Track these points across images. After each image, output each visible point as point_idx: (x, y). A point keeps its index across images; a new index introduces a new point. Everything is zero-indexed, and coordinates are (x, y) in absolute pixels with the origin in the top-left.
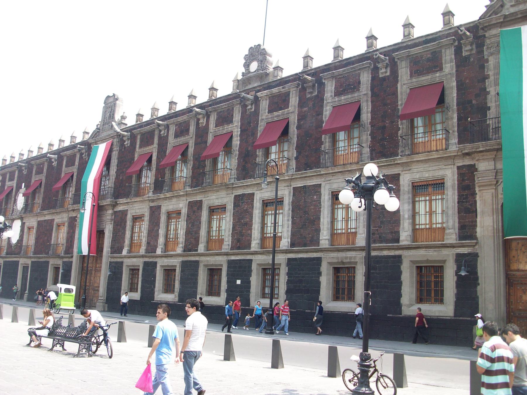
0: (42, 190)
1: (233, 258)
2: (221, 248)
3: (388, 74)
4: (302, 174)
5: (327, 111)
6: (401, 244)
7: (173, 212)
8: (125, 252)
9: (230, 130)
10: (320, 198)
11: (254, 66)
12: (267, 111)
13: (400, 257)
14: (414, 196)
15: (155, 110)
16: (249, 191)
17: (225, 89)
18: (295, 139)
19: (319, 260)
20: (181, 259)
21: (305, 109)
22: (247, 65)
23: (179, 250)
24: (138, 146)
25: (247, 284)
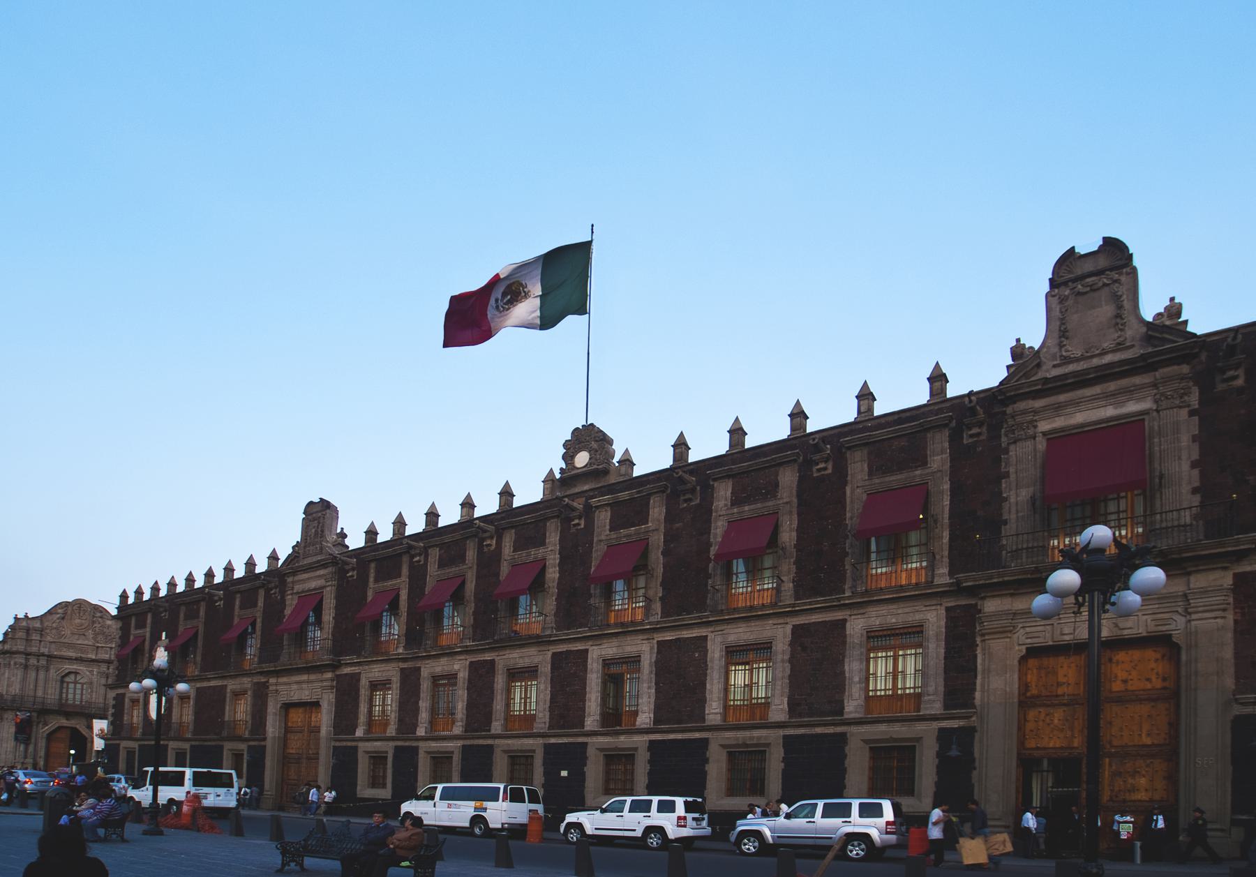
0: (200, 643)
1: (553, 741)
2: (385, 732)
3: (829, 471)
5: (719, 528)
6: (846, 716)
7: (443, 677)
8: (359, 733)
9: (540, 556)
10: (706, 655)
11: (582, 459)
13: (844, 735)
14: (728, 664)
16: (579, 646)
18: (660, 570)
19: (705, 742)
20: (460, 743)
22: (568, 457)
23: (458, 730)
24: (371, 579)
25: (578, 777)
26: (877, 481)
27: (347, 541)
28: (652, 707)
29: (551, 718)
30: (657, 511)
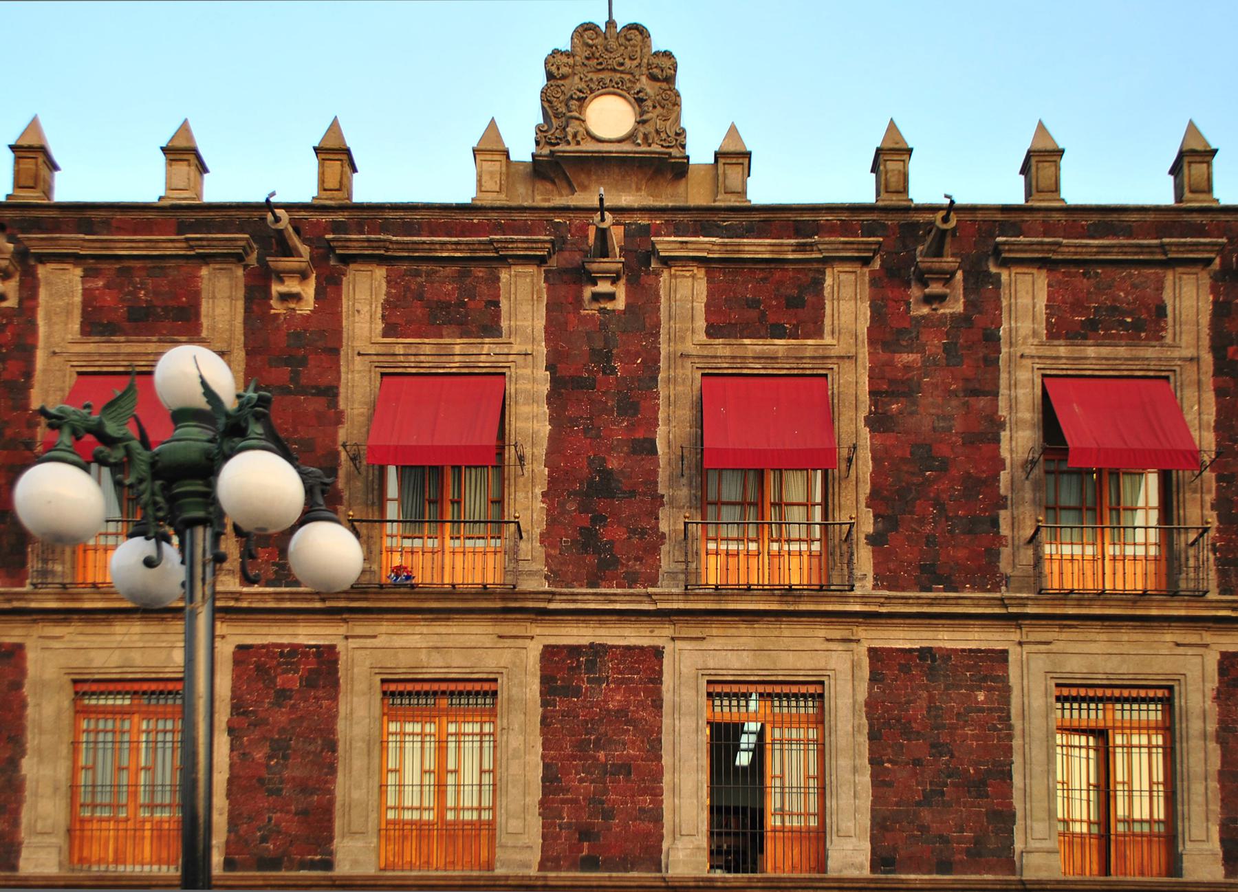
4: (933, 602)
12: (701, 324)
15: (490, 149)
17: (420, 165)
18: (865, 465)
21: (907, 358)
26: (1063, 351)
27: (514, 157)
28: (866, 820)
29: (547, 837)
30: (847, 305)
